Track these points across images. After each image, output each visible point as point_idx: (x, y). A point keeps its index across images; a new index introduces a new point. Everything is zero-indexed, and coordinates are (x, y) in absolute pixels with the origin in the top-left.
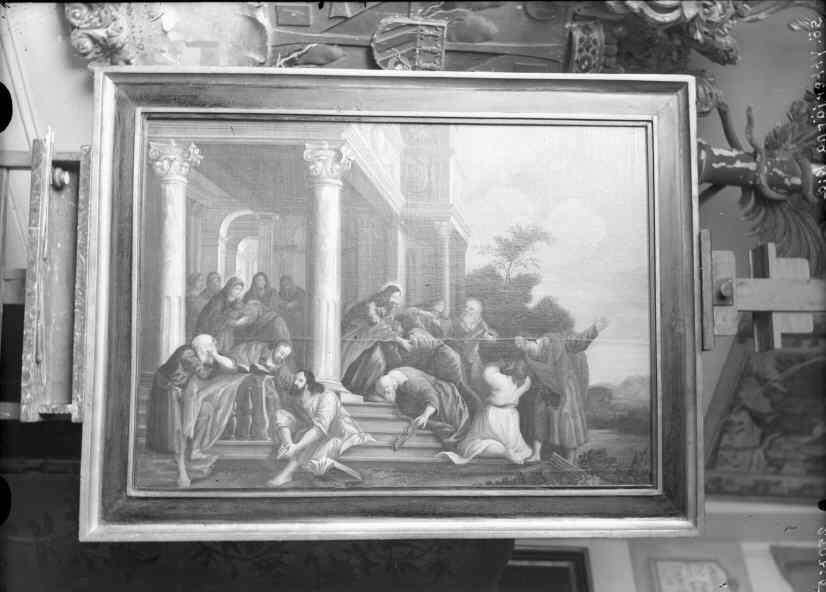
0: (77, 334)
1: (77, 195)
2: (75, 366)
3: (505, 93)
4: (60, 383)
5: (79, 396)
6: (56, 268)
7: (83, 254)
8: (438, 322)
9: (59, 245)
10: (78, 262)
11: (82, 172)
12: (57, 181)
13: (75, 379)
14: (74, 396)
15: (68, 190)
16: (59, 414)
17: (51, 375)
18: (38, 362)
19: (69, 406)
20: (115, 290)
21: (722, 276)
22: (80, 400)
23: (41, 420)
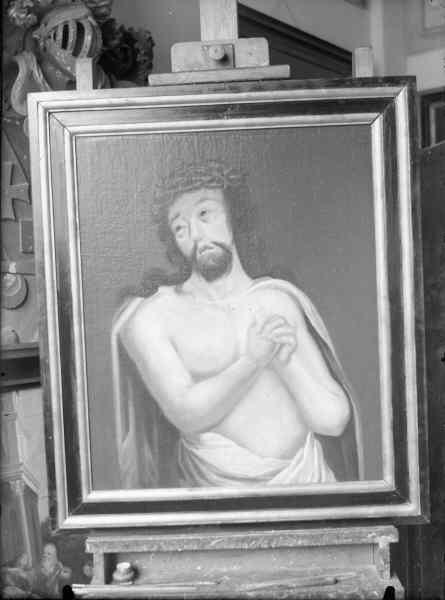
0: (300, 543)
1: (143, 553)
2: (336, 542)
3: (45, 455)
4: (351, 556)
5: (370, 536)
6: (225, 570)
7: (209, 543)
8: (24, 575)
9: (199, 568)
10: (217, 547)
11: (115, 551)
12: (128, 576)
13: (350, 541)
14: (370, 542)
15: (137, 562)
16: (391, 557)
17: (342, 566)
18: (336, 582)
19: (381, 546)
20: (427, 500)
21: (200, 58)
22: (374, 534)
23: (395, 574)
